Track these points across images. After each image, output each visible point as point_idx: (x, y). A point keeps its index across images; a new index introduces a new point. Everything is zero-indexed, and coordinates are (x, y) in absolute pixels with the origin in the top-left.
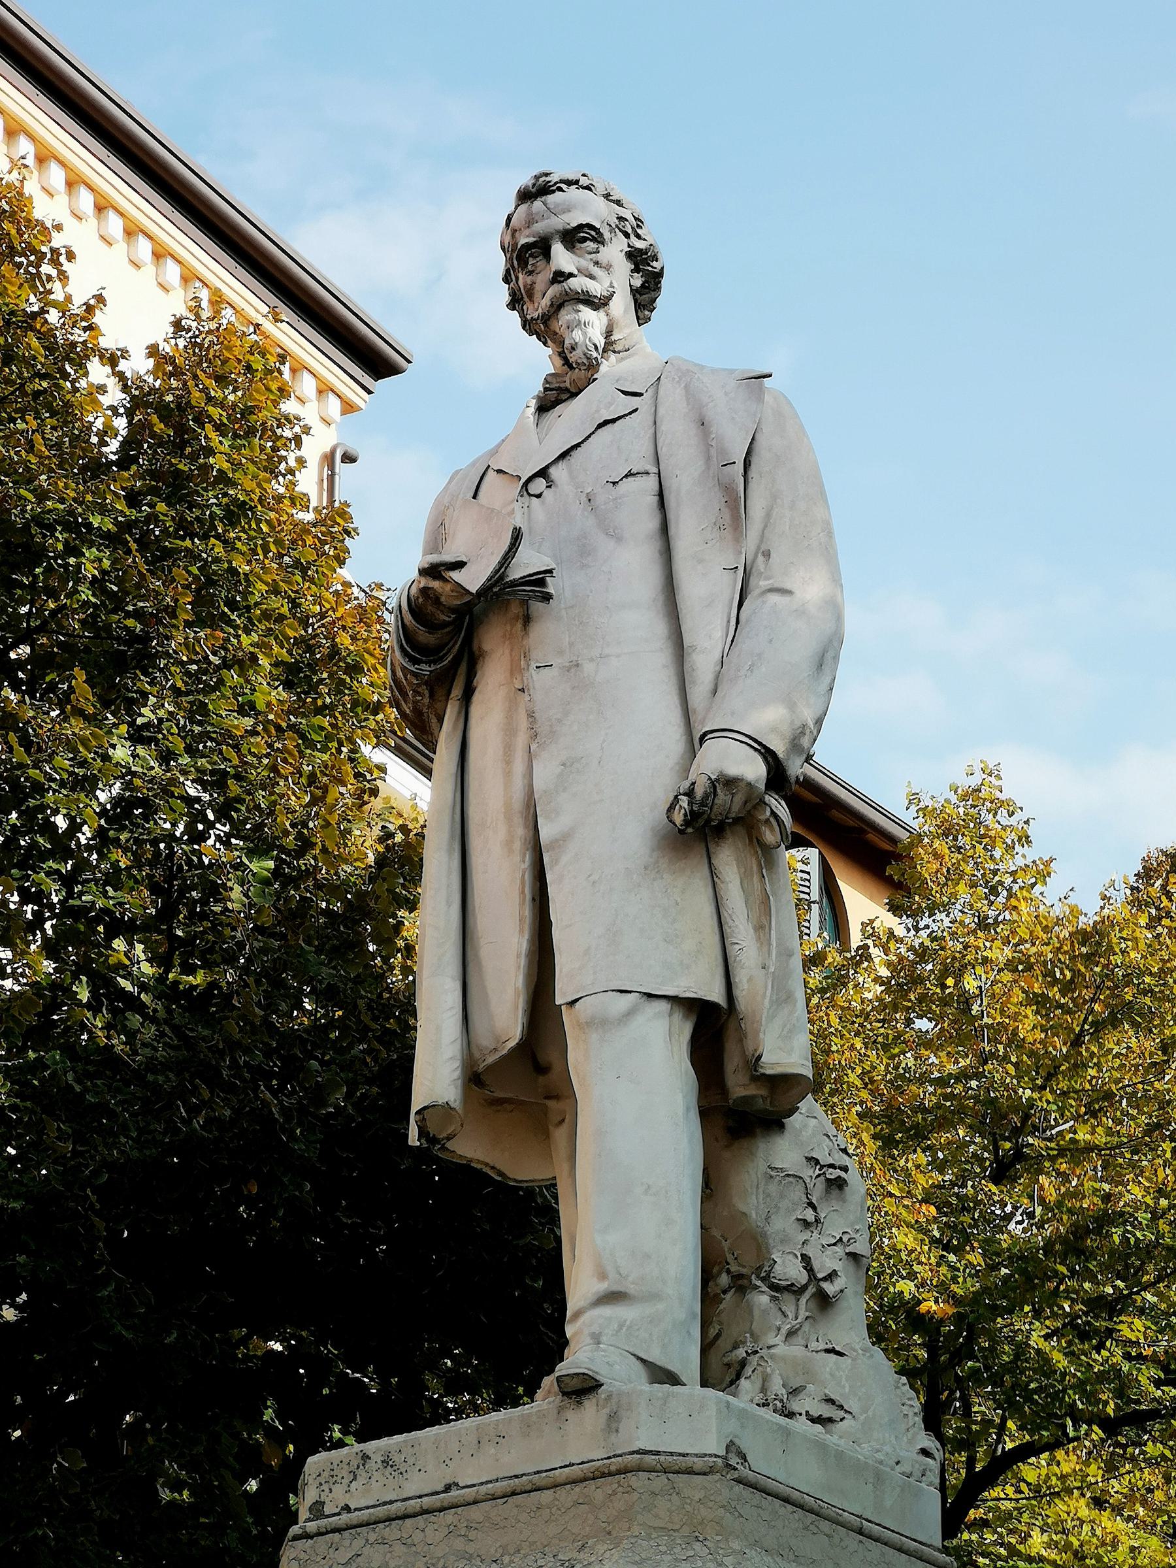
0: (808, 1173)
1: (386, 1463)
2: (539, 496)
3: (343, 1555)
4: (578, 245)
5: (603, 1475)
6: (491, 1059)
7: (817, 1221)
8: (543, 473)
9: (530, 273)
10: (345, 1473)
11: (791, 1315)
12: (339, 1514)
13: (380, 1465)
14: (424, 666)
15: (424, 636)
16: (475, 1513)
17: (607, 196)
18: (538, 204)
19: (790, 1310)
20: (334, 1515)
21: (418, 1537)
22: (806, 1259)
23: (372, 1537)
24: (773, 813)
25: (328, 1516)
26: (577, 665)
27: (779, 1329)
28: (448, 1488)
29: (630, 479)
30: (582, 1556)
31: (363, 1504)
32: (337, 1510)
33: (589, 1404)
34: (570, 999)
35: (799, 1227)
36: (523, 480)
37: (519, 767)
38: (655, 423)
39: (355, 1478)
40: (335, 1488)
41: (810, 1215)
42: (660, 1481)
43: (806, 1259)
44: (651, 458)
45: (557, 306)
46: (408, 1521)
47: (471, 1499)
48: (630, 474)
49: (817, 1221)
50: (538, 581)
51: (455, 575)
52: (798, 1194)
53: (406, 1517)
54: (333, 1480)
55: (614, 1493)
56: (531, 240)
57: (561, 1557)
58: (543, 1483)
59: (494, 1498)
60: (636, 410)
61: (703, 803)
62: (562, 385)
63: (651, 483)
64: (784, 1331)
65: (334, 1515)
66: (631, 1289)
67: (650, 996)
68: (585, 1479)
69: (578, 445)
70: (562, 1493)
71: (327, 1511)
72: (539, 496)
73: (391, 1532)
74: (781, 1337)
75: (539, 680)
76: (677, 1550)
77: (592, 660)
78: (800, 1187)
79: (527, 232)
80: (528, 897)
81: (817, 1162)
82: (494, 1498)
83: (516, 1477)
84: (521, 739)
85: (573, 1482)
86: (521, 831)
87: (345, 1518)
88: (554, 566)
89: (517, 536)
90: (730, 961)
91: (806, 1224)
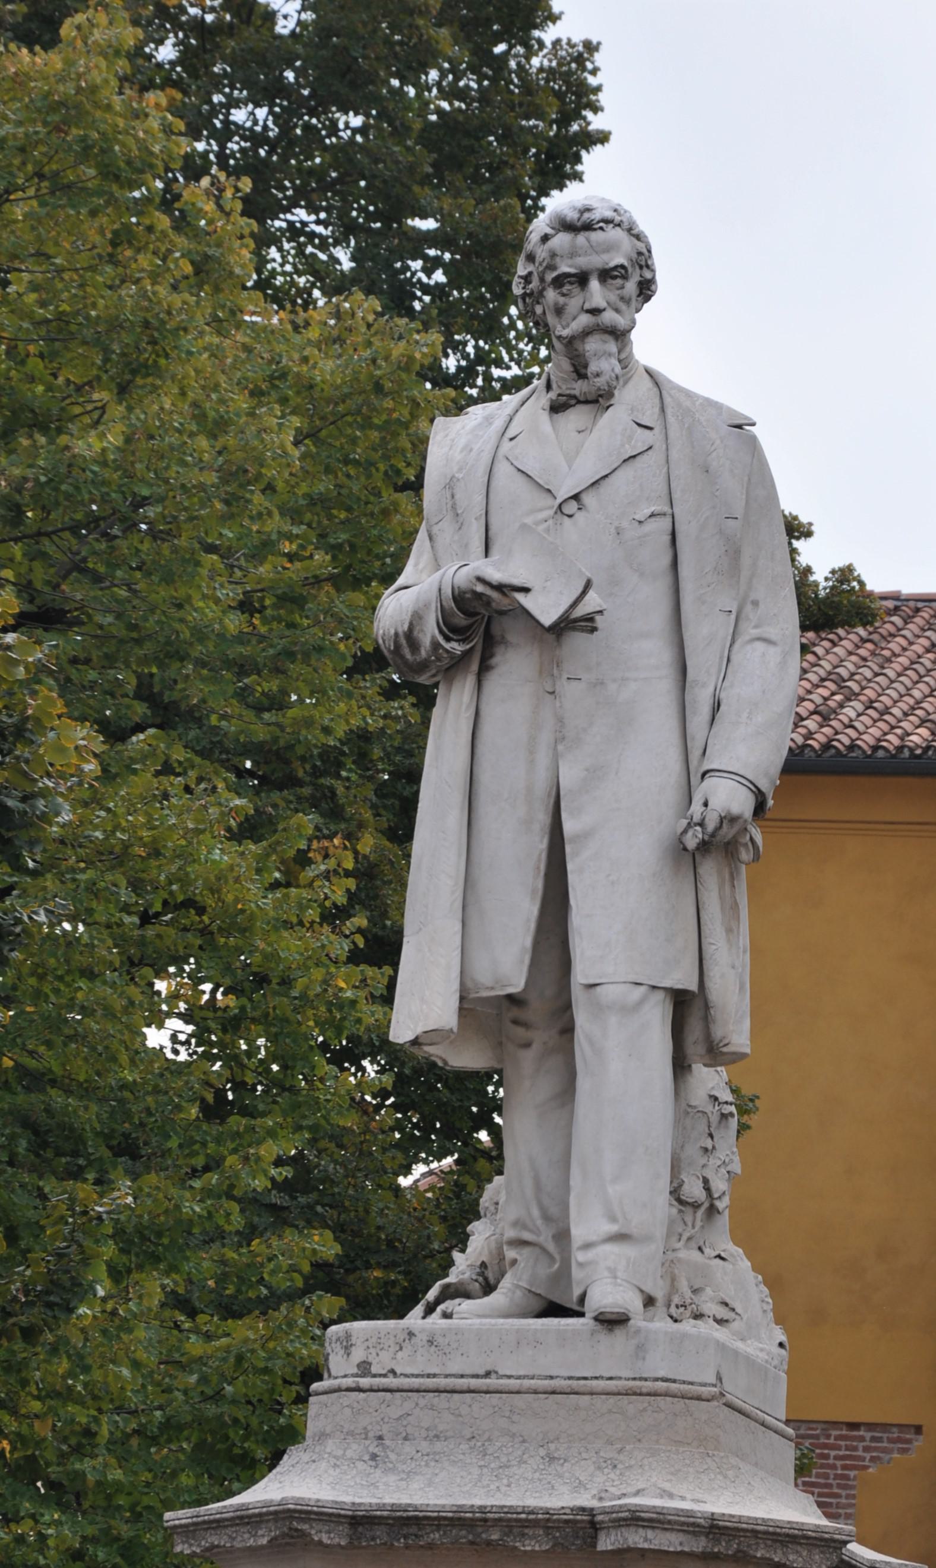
0: (709, 1108)
1: (431, 1342)
2: (570, 516)
3: (395, 1412)
4: (610, 281)
5: (635, 1394)
6: (485, 994)
7: (714, 1148)
8: (576, 497)
9: (564, 295)
10: (391, 1342)
11: (690, 1224)
12: (385, 1376)
13: (425, 1342)
14: (454, 645)
15: (461, 620)
17: (629, 230)
18: (581, 239)
19: (689, 1219)
20: (381, 1375)
21: (464, 1410)
22: (706, 1181)
23: (422, 1402)
24: (751, 839)
25: (375, 1376)
26: (602, 683)
27: (681, 1235)
28: (488, 1374)
29: (653, 519)
30: (621, 1457)
31: (409, 1370)
32: (384, 1372)
33: (619, 1333)
34: (592, 981)
35: (701, 1153)
36: (559, 501)
37: (543, 760)
38: (667, 462)
39: (401, 1349)
40: (382, 1354)
41: (709, 1144)
42: (680, 1404)
43: (706, 1181)
44: (666, 499)
45: (586, 333)
46: (456, 1396)
47: (516, 1389)
48: (652, 515)
49: (714, 1148)
50: (589, 618)
51: (520, 597)
52: (703, 1127)
54: (379, 1346)
55: (645, 1410)
56: (572, 270)
57: (602, 1454)
58: (581, 1390)
59: (536, 1392)
61: (713, 835)
62: (572, 392)
63: (665, 524)
64: (684, 1238)
65: (381, 1375)
67: (654, 987)
68: (619, 1394)
69: (606, 476)
70: (598, 1400)
71: (374, 1370)
72: (570, 516)
73: (441, 1400)
74: (682, 1242)
75: (571, 692)
76: (697, 1463)
77: (614, 681)
78: (705, 1121)
79: (570, 262)
80: (542, 873)
81: (716, 1099)
82: (536, 1392)
83: (551, 1378)
84: (546, 737)
85: (608, 1394)
86: (542, 818)
87: (390, 1381)
88: (604, 607)
89: (588, 585)
90: (705, 955)
91: (706, 1150)
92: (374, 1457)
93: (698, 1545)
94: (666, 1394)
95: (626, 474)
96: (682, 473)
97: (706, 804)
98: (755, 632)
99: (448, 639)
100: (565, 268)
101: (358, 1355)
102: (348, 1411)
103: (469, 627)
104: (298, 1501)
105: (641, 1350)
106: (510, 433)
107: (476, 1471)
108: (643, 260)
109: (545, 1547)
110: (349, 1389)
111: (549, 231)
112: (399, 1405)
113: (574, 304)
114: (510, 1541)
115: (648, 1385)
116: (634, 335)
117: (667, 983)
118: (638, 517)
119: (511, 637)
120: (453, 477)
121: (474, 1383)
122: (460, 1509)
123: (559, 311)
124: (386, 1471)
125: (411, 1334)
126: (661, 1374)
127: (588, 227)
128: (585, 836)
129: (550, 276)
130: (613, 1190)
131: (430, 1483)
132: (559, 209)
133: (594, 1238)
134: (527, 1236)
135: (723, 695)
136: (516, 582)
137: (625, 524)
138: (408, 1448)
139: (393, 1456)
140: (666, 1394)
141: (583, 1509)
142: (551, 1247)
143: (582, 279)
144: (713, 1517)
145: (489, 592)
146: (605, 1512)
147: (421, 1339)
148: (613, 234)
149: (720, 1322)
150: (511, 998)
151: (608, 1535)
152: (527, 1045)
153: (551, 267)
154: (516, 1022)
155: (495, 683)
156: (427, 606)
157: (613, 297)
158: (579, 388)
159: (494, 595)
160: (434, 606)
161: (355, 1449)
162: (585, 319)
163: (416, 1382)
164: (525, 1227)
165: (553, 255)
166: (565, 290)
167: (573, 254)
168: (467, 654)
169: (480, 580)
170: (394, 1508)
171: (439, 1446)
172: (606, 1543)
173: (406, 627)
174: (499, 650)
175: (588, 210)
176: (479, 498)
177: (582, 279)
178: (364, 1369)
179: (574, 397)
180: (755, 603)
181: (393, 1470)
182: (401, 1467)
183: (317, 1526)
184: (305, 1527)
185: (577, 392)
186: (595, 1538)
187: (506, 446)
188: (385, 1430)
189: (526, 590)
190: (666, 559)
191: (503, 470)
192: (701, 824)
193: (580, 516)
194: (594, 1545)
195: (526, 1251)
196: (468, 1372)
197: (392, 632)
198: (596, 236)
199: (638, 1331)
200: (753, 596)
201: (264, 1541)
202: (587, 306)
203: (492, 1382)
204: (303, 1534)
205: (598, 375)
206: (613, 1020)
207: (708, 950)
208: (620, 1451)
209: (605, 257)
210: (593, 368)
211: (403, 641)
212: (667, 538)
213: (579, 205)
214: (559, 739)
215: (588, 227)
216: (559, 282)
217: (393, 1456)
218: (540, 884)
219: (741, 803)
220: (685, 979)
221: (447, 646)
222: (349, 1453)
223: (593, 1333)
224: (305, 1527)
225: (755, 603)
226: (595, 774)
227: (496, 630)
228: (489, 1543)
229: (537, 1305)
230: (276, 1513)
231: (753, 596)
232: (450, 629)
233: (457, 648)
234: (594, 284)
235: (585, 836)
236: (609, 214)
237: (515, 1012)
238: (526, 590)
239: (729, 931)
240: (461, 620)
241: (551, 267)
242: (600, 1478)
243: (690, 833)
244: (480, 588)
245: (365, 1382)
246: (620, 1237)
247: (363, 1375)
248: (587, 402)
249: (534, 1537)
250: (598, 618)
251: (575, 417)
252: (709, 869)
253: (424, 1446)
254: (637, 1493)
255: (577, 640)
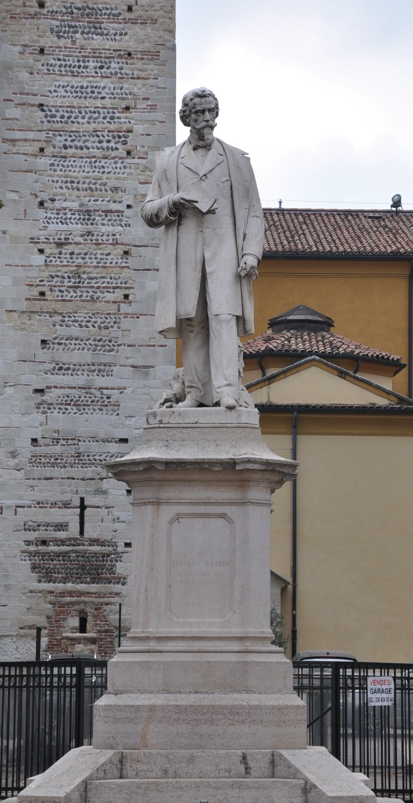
1: (179, 414)
3: (171, 434)
8: (205, 175)
16: (206, 430)
18: (203, 100)
21: (191, 433)
23: (178, 431)
28: (196, 423)
33: (233, 411)
45: (204, 127)
50: (214, 210)
51: (195, 204)
53: (187, 428)
56: (201, 109)
59: (211, 427)
60: (4, 100)
63: (229, 183)
66: (232, 383)
70: (229, 429)
73: (184, 430)
82: (211, 427)
84: (200, 245)
86: (200, 267)
87: (168, 425)
92: (167, 446)
93: (263, 467)
94: (248, 427)
95: (217, 169)
96: (232, 168)
97: (245, 263)
98: (254, 214)
99: (170, 216)
100: (199, 108)
101: (159, 418)
102: (157, 434)
103: (175, 213)
104: (153, 458)
105: (239, 416)
106: (182, 156)
107: (196, 449)
108: (217, 107)
109: (221, 469)
110: (157, 428)
111: (193, 97)
112: (171, 432)
113: (201, 118)
114: (211, 468)
115: (242, 425)
116: (215, 128)
117: (236, 314)
118: (223, 181)
119: (188, 216)
120: (165, 169)
121: (193, 425)
122: (197, 459)
123: (196, 121)
124: (171, 450)
125: (174, 412)
126: (245, 422)
127: (205, 96)
128: (212, 273)
129: (193, 110)
130: (226, 372)
131: (185, 453)
132: (195, 91)
133: (221, 385)
134: (193, 385)
135: (246, 232)
136: (194, 199)
137: (219, 183)
138: (176, 443)
139: (172, 446)
140: (248, 427)
141: (232, 459)
142: (201, 388)
143: (203, 112)
144: (267, 460)
145: (185, 202)
146: (238, 459)
147: (177, 414)
148: (211, 98)
149: (246, 407)
150: (188, 319)
151: (240, 465)
152: (192, 332)
153: (195, 108)
154: (188, 325)
155: (182, 228)
156: (164, 206)
157: (211, 117)
158: (201, 143)
159: (187, 203)
160: (167, 206)
161: (161, 444)
162: (204, 123)
163: (176, 425)
164: (192, 382)
165: (195, 104)
166: (198, 114)
167: (201, 104)
168: (175, 220)
169: (182, 199)
170: (178, 459)
171: (185, 443)
172: (238, 467)
173: (156, 212)
174: (184, 219)
175: (204, 91)
176: (175, 175)
177: (203, 112)
178: (161, 422)
179: (199, 146)
180: (253, 206)
181: (173, 449)
182: (175, 448)
183: (158, 465)
184: (155, 465)
185: (200, 144)
186: (235, 466)
187: (181, 160)
188: (168, 439)
189: (197, 202)
190: (230, 193)
191: (181, 167)
192: (245, 269)
193: (206, 180)
194: (235, 468)
195: (193, 389)
196: (190, 422)
197: (150, 214)
198: (207, 99)
199: (238, 410)
200: (252, 204)
201: (142, 469)
202: (205, 119)
203: (197, 425)
204: (154, 467)
205: (208, 139)
206: (224, 324)
207: (245, 305)
208: (237, 443)
209: (210, 105)
210: (206, 137)
211: (154, 217)
212: (230, 187)
213: (202, 89)
214: (204, 244)
215: (205, 96)
216: (196, 112)
217: (172, 446)
218: (199, 286)
219: (255, 263)
220: (239, 313)
221: (171, 218)
222: (159, 445)
223: (226, 411)
224: (155, 465)
225: (253, 206)
226: (214, 255)
227: (183, 213)
228: (205, 468)
229: (197, 404)
230: (146, 461)
231: (252, 204)
232: (171, 213)
233: (172, 218)
234: (207, 113)
235: (212, 273)
236: (210, 93)
237: (189, 323)
238: (197, 202)
239: (250, 299)
240: (174, 210)
241: (194, 108)
242: (232, 450)
243: (242, 272)
244: (182, 201)
245: (162, 425)
246: (229, 385)
247: (161, 424)
248: (203, 147)
249: (217, 466)
250: (216, 210)
251: (200, 152)
252: (244, 282)
253: (181, 443)
254: (245, 454)
255: (210, 216)
